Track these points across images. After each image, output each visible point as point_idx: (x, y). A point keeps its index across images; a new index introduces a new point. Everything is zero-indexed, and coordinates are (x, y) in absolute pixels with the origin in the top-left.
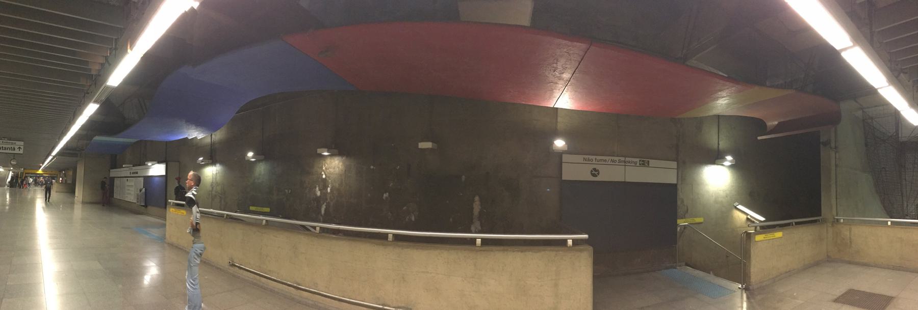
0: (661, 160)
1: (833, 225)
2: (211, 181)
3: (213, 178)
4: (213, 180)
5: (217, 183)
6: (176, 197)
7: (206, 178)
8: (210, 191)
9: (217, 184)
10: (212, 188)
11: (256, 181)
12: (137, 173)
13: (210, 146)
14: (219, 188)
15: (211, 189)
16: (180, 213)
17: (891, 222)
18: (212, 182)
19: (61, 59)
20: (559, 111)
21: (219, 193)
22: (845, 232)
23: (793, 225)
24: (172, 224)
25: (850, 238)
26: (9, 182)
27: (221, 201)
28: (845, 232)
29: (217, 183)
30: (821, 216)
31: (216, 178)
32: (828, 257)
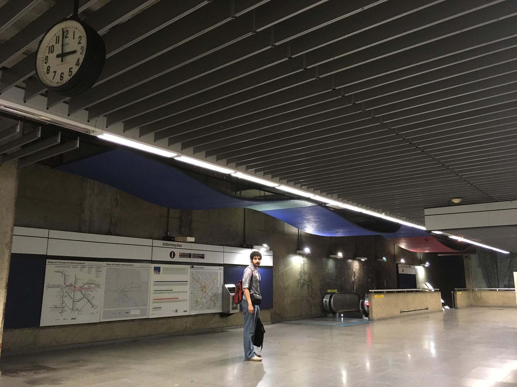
0: (32, 228)
1: (472, 292)
2: (299, 270)
3: (301, 269)
4: (301, 270)
5: (305, 272)
6: (488, 287)
7: (294, 267)
8: (299, 280)
9: (305, 273)
10: (301, 277)
11: (329, 272)
12: (202, 257)
13: (297, 237)
14: (306, 277)
15: (300, 277)
16: (380, 297)
17: (477, 289)
18: (301, 272)
19: (366, 148)
20: (401, 228)
21: (306, 281)
22: (479, 294)
23: (414, 292)
24: (376, 306)
25: (481, 297)
26: (352, 276)
27: (308, 288)
28: (479, 294)
29: (305, 272)
30: (466, 288)
31: (304, 268)
32: (471, 305)
